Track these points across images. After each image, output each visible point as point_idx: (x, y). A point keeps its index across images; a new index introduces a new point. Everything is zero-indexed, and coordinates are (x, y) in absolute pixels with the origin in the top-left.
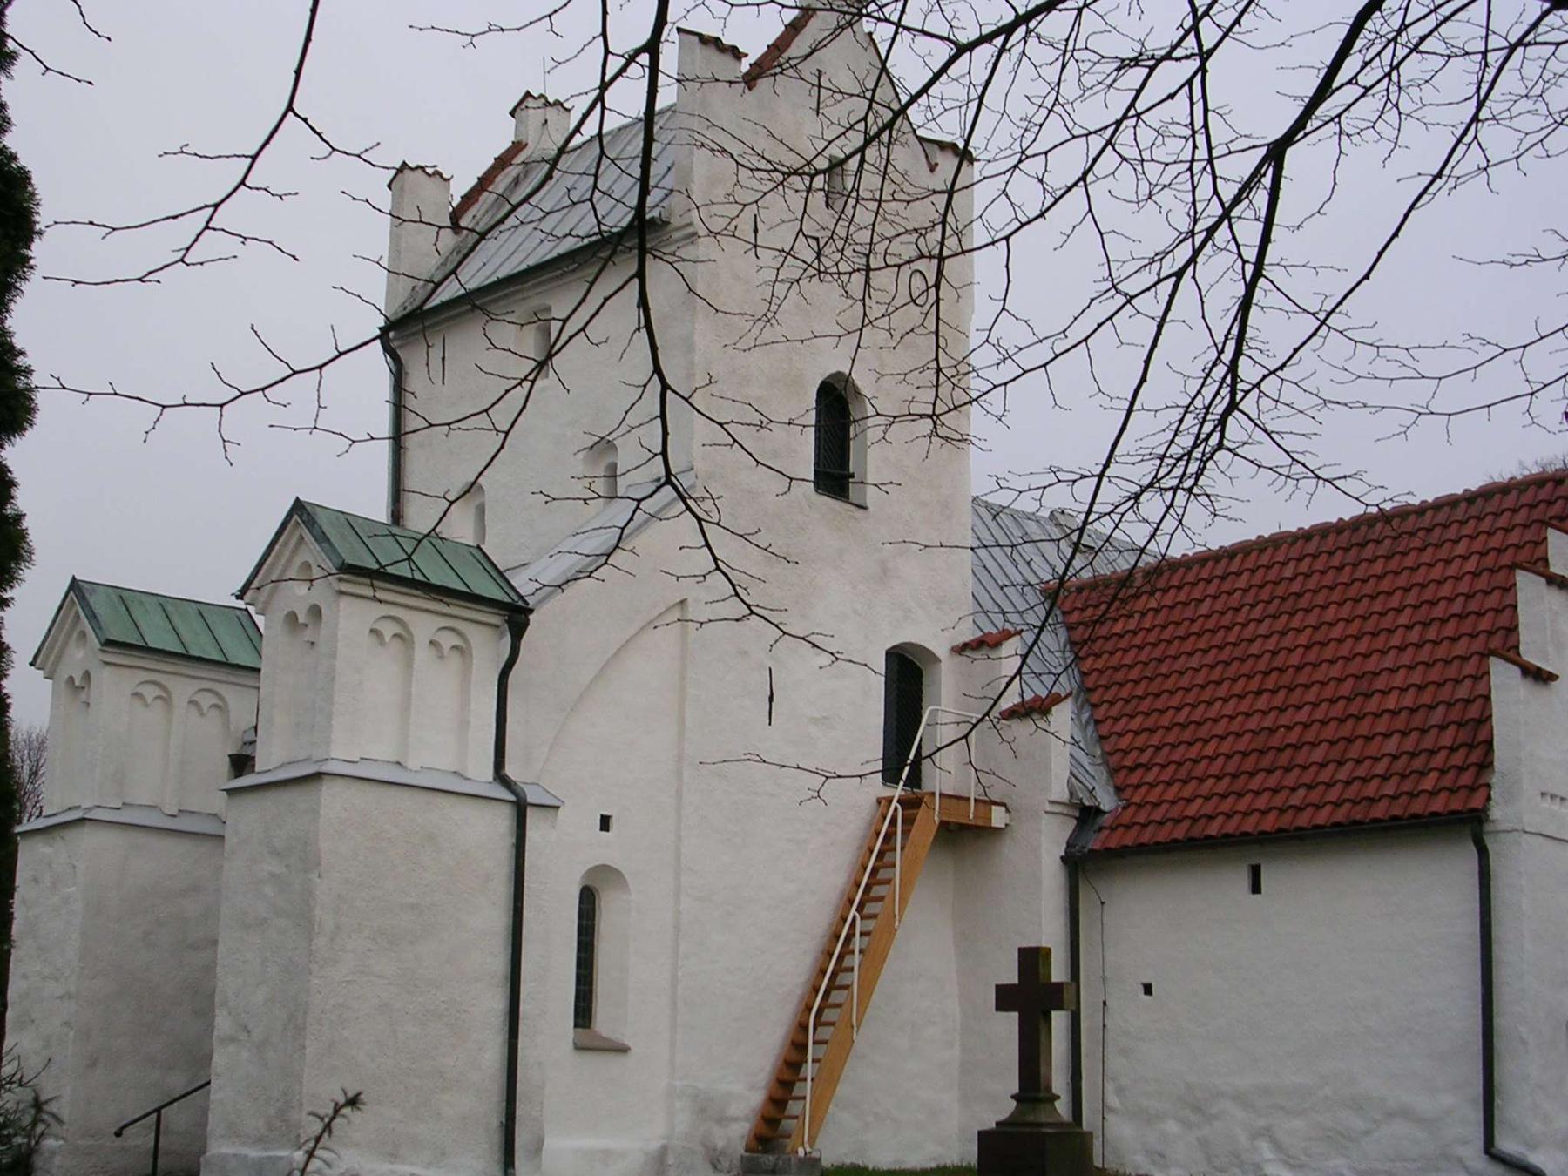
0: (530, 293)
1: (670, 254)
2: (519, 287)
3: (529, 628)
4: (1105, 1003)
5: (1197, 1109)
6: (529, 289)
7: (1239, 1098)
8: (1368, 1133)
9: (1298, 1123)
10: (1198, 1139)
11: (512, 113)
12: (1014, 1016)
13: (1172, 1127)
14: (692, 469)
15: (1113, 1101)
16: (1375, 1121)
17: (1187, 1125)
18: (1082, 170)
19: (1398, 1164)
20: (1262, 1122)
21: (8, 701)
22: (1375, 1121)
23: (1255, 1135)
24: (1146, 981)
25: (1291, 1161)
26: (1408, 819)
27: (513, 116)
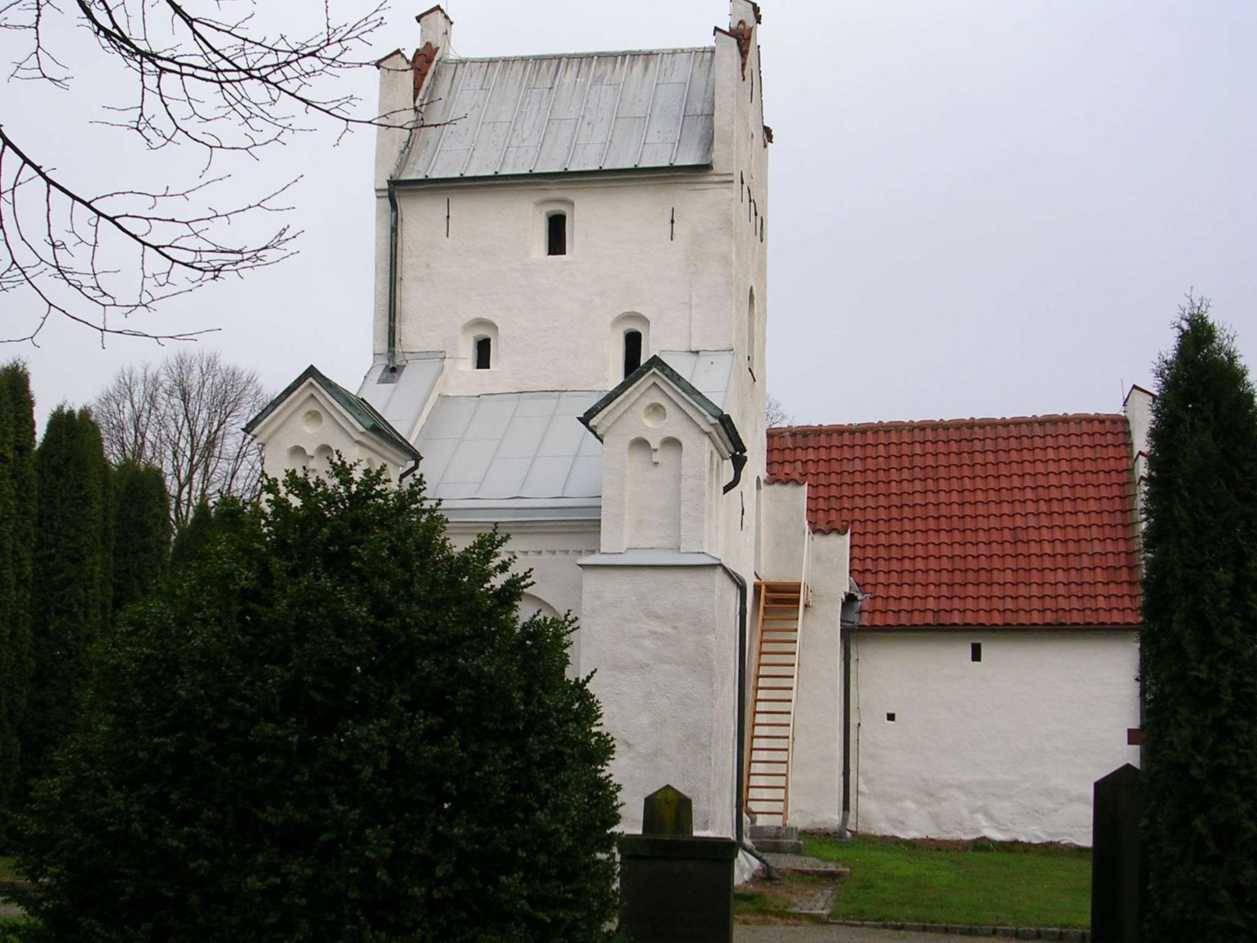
0: (554, 187)
1: (167, 59)
2: (547, 181)
3: (747, 463)
4: (859, 725)
5: (930, 794)
6: (555, 184)
7: (962, 787)
8: (1055, 810)
9: (1007, 804)
10: (930, 814)
11: (419, 19)
12: (1137, 747)
13: (910, 805)
14: (732, 350)
15: (862, 788)
16: (1060, 804)
17: (920, 804)
18: (196, 17)
19: (1077, 829)
20: (980, 803)
21: (66, 410)
22: (1060, 804)
23: (973, 812)
24: (890, 712)
25: (1001, 827)
26: (1069, 625)
27: (419, 21)
